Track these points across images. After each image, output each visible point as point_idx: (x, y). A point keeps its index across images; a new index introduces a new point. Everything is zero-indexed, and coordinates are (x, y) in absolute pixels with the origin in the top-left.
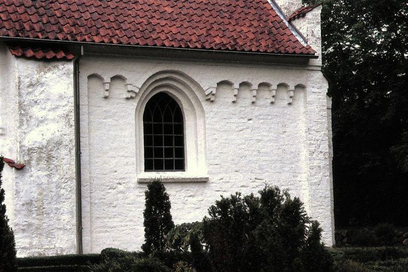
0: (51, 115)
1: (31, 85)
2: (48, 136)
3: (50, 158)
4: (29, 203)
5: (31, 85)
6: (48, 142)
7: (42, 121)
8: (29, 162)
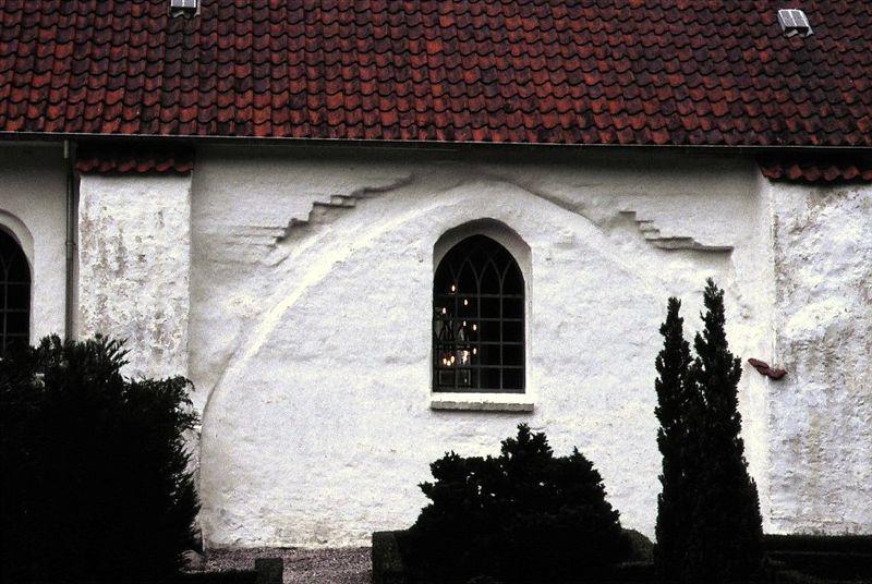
0: (833, 283)
1: (797, 229)
2: (828, 319)
3: (830, 360)
4: (794, 440)
5: (797, 229)
6: (828, 330)
7: (815, 294)
8: (794, 366)
